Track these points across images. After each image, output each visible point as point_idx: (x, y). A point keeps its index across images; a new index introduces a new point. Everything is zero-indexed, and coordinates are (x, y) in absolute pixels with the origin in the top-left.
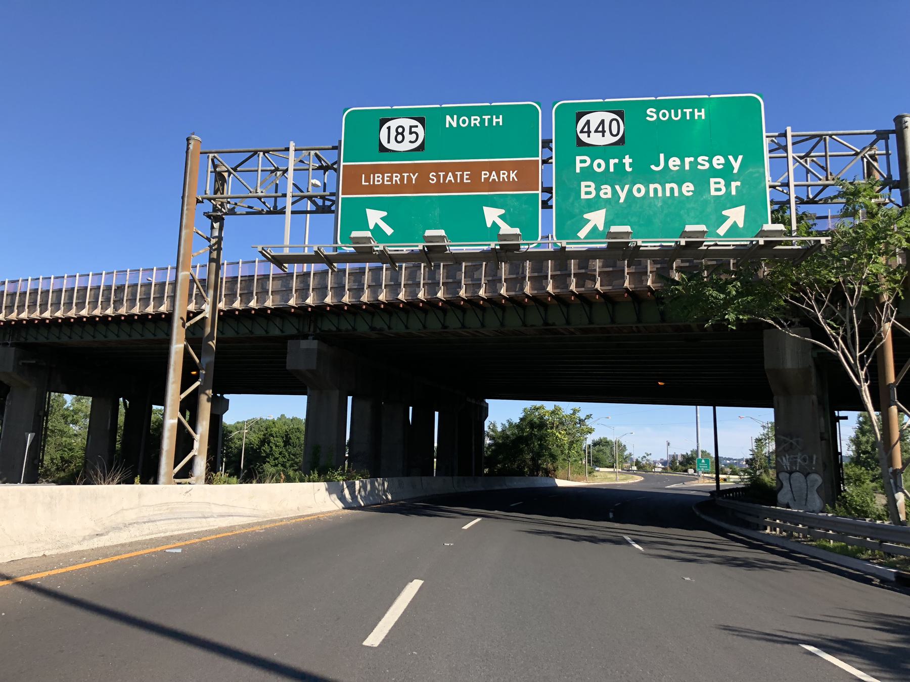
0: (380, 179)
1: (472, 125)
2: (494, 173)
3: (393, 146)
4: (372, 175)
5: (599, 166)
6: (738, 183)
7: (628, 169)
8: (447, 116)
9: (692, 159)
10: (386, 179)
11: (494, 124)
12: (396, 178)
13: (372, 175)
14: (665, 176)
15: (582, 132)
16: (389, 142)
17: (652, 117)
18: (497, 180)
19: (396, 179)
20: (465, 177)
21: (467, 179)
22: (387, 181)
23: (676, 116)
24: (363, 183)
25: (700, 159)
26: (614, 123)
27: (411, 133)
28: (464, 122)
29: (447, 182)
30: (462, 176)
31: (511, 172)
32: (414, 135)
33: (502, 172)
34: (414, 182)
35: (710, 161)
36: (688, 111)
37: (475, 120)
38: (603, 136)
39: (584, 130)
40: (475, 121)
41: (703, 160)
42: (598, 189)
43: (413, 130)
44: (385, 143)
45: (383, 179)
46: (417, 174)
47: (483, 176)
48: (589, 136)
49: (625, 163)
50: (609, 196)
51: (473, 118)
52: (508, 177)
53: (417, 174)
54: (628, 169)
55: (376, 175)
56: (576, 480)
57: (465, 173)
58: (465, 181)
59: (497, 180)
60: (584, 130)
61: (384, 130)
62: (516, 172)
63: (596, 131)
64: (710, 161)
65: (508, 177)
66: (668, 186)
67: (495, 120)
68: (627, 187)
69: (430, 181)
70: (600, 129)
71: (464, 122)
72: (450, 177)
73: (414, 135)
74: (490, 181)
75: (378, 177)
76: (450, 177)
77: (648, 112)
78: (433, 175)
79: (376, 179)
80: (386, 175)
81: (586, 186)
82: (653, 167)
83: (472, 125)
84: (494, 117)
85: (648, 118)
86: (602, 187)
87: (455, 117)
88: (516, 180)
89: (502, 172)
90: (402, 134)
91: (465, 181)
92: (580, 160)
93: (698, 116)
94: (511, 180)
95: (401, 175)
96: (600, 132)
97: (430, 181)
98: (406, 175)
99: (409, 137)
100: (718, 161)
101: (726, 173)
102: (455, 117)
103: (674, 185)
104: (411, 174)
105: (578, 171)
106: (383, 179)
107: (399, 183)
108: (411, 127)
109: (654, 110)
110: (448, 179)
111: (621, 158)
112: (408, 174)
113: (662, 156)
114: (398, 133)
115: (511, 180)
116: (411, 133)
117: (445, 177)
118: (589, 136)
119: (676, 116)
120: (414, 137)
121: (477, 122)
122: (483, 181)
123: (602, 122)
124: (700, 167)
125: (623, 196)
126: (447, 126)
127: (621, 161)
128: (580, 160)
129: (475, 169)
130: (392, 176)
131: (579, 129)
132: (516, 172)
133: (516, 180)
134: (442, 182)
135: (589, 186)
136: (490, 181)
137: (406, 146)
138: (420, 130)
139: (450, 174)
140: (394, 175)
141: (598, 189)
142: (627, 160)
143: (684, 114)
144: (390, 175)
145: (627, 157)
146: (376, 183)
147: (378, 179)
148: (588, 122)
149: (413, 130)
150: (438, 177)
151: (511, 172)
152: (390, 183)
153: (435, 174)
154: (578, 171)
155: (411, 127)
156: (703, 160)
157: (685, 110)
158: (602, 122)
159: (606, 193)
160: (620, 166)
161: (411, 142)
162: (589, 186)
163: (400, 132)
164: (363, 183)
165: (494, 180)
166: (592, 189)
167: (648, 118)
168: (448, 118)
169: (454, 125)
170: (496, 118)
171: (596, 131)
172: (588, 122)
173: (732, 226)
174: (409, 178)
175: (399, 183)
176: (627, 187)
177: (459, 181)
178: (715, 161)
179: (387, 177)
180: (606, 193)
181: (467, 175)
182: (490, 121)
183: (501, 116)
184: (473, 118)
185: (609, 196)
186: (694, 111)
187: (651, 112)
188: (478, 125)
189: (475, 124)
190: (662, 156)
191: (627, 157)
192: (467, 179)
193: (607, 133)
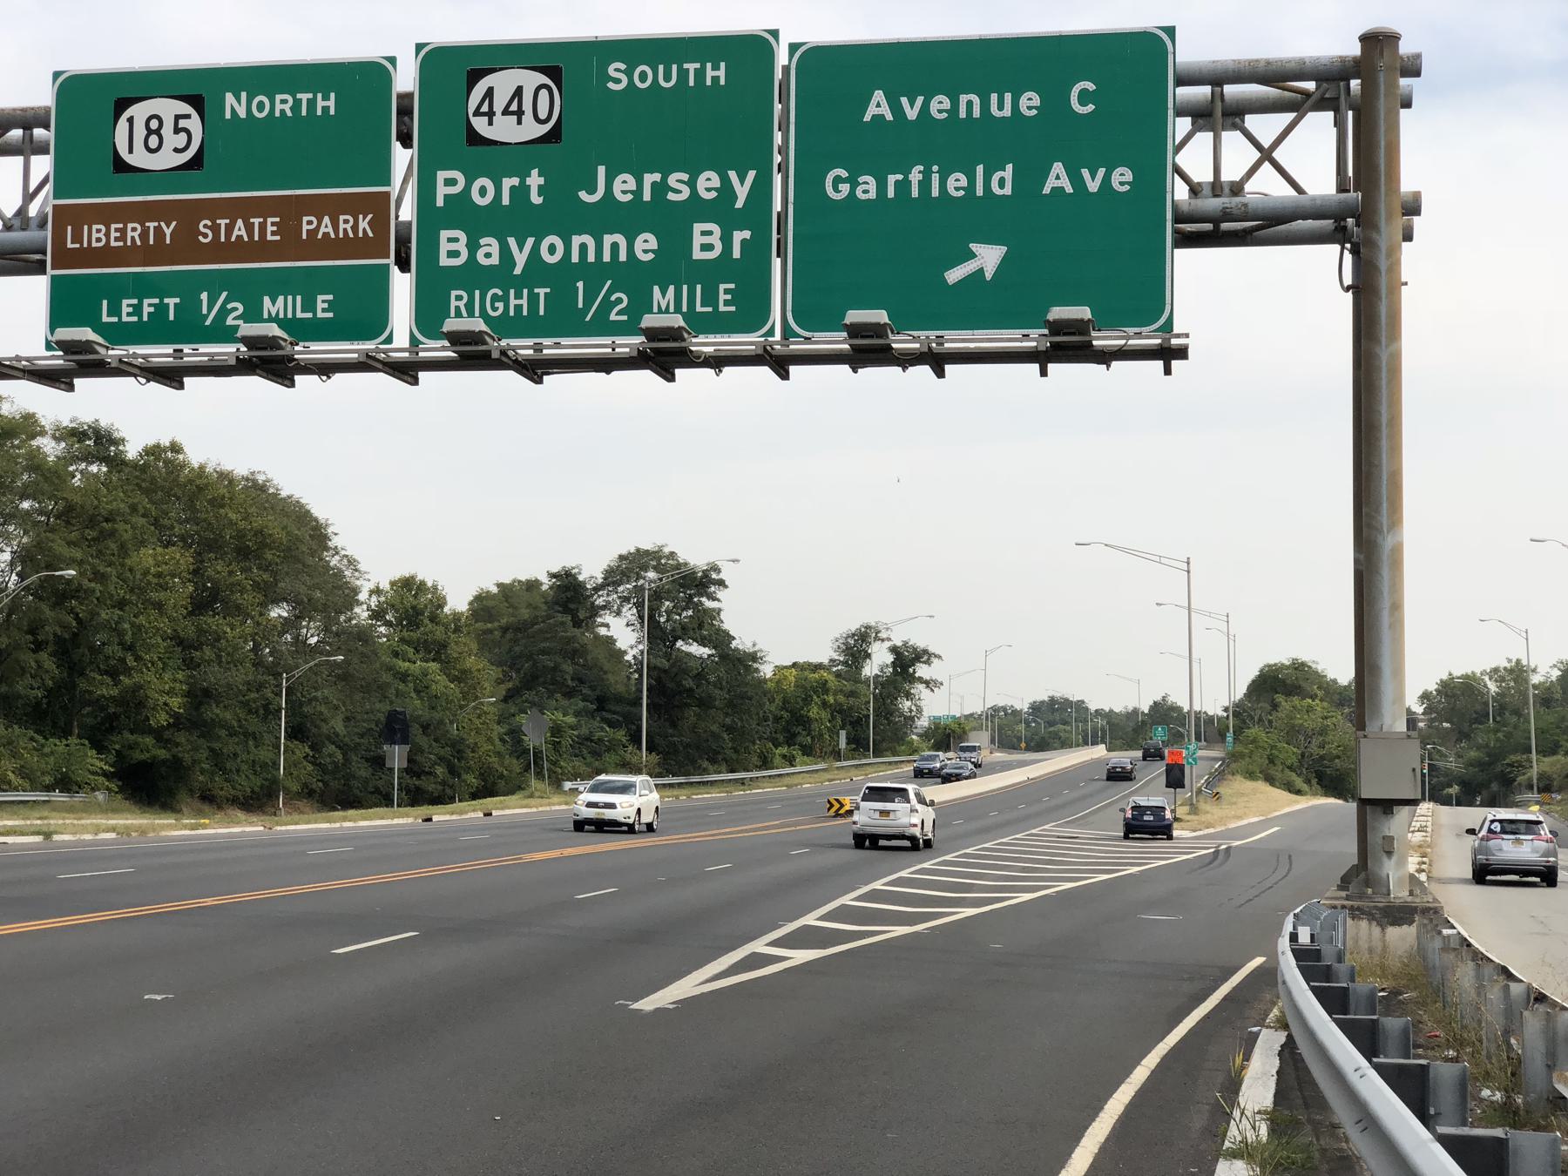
0: (101, 235)
1: (277, 114)
2: (326, 219)
3: (139, 158)
4: (86, 227)
5: (483, 192)
6: (747, 234)
7: (536, 199)
8: (227, 94)
9: (657, 177)
10: (114, 235)
11: (709, 82)
12: (134, 232)
13: (86, 227)
14: (609, 216)
15: (477, 113)
16: (131, 151)
17: (618, 81)
18: (333, 236)
19: (458, 303)
20: (270, 228)
21: (273, 233)
22: (116, 239)
23: (667, 78)
24: (70, 245)
25: (672, 180)
26: (544, 93)
27: (177, 130)
28: (261, 106)
29: (233, 239)
30: (263, 227)
31: (361, 217)
32: (183, 136)
33: (342, 218)
34: (168, 242)
35: (692, 184)
36: (692, 67)
37: (284, 102)
38: (519, 122)
39: (511, 109)
40: (283, 104)
41: (677, 181)
42: (473, 246)
43: (182, 123)
44: (123, 151)
45: (107, 235)
46: (174, 223)
47: (305, 227)
48: (490, 123)
49: (530, 186)
50: (495, 260)
51: (279, 97)
52: (355, 228)
53: (174, 223)
54: (536, 199)
55: (95, 227)
56: (222, 788)
57: (270, 220)
58: (270, 237)
59: (333, 236)
60: (511, 109)
61: (122, 124)
62: (370, 216)
63: (506, 112)
64: (692, 184)
65: (355, 228)
66: (608, 240)
67: (710, 73)
68: (530, 241)
69: (201, 238)
70: (514, 107)
71: (261, 106)
72: (240, 230)
73: (183, 136)
74: (320, 236)
75: (99, 231)
76: (240, 230)
77: (611, 71)
78: (205, 226)
79: (95, 235)
80: (113, 226)
81: (450, 240)
82: (583, 195)
83: (277, 114)
84: (709, 65)
85: (611, 85)
86: (483, 241)
87: (244, 95)
88: (371, 235)
89: (342, 218)
90: (158, 132)
91: (270, 237)
92: (445, 179)
93: (718, 69)
94: (361, 235)
95: (142, 225)
96: (513, 113)
97: (201, 238)
98: (152, 225)
99: (172, 140)
100: (708, 183)
101: (721, 210)
102: (244, 95)
103: (620, 239)
104: (163, 224)
106: (107, 235)
107: (139, 243)
108: (178, 118)
109: (623, 67)
110: (236, 233)
112: (156, 224)
113: (601, 170)
114: (150, 132)
115: (361, 235)
116: (177, 130)
117: (230, 228)
118: (490, 123)
119: (667, 78)
120: (181, 139)
121: (287, 107)
122: (304, 237)
123: (519, 92)
124: (671, 196)
125: (521, 259)
126: (228, 116)
127: (523, 182)
128: (445, 179)
129: (291, 211)
130: (125, 228)
131: (471, 112)
132: (370, 216)
133: (371, 235)
134: (223, 239)
135: (456, 240)
136: (320, 236)
137: (167, 159)
138: (194, 124)
139: (240, 223)
140: (130, 226)
141: (473, 246)
142: (535, 180)
143: (683, 74)
144: (121, 226)
145: (535, 172)
146: (94, 244)
147: (98, 235)
148: (490, 93)
149: (182, 123)
150: (215, 229)
151: (361, 217)
152: (121, 244)
153: (209, 223)
155: (178, 118)
156: (677, 181)
157: (686, 66)
158: (519, 92)
159: (488, 255)
160: (520, 192)
161: (176, 150)
162: (456, 240)
163: (154, 129)
164: (70, 245)
165: (326, 235)
166: (461, 247)
167: (611, 85)
169: (242, 113)
171: (506, 112)
172: (490, 93)
173: (386, 264)
174: (158, 230)
175: (139, 243)
176: (530, 241)
177: (256, 238)
178: (701, 184)
180: (488, 255)
181: (273, 224)
182: (700, 74)
183: (723, 65)
184: (279, 97)
185: (495, 260)
187: (617, 70)
188: (289, 114)
190: (601, 170)
191: (535, 172)
192: (273, 233)
193: (528, 116)
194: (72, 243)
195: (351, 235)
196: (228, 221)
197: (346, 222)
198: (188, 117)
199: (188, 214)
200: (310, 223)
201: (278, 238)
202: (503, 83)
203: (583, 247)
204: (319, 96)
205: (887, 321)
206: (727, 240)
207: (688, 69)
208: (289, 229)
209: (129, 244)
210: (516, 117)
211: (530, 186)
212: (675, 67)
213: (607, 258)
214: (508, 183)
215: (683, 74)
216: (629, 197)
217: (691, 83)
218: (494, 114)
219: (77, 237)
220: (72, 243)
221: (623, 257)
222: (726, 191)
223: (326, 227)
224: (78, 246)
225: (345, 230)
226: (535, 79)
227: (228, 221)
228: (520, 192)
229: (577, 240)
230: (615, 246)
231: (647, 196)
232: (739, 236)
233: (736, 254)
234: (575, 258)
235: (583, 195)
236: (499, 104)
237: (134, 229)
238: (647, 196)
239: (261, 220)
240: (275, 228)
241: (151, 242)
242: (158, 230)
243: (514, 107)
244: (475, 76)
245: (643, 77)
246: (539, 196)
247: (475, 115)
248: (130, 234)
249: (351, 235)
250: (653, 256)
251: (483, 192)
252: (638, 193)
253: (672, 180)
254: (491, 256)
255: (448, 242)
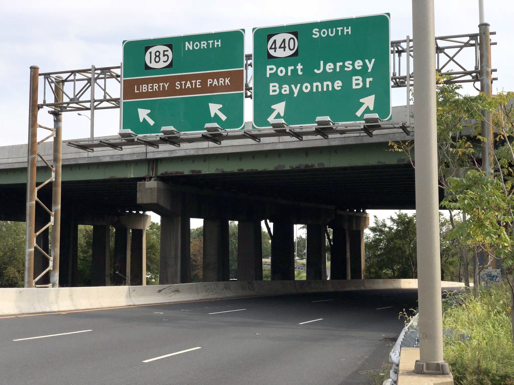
0: (146, 88)
1: (202, 48)
2: (215, 80)
3: (153, 65)
4: (141, 86)
5: (281, 72)
6: (371, 79)
7: (300, 73)
9: (341, 64)
10: (149, 88)
12: (156, 86)
13: (141, 86)
14: (325, 77)
15: (271, 48)
16: (151, 63)
17: (316, 35)
18: (217, 85)
20: (198, 84)
21: (199, 85)
22: (150, 89)
23: (332, 33)
24: (136, 92)
25: (346, 64)
26: (292, 41)
27: (164, 55)
28: (197, 46)
30: (196, 83)
31: (226, 79)
32: (166, 57)
33: (220, 79)
35: (353, 65)
36: (340, 29)
38: (284, 50)
42: (280, 88)
43: (166, 53)
45: (148, 88)
46: (168, 83)
47: (209, 83)
48: (275, 51)
49: (298, 69)
50: (288, 92)
51: (202, 43)
52: (224, 82)
53: (168, 83)
54: (300, 73)
55: (144, 86)
57: (198, 81)
58: (198, 87)
59: (217, 85)
61: (148, 55)
63: (280, 47)
64: (353, 65)
65: (224, 82)
66: (325, 84)
67: (346, 30)
68: (299, 85)
69: (176, 88)
70: (283, 46)
72: (188, 84)
73: (166, 57)
74: (213, 85)
75: (145, 87)
76: (188, 84)
77: (314, 32)
78: (178, 84)
79: (144, 88)
80: (149, 85)
82: (316, 71)
83: (202, 48)
85: (314, 36)
86: (283, 86)
88: (229, 84)
89: (220, 79)
90: (159, 56)
91: (198, 87)
94: (226, 84)
95: (158, 84)
96: (282, 48)
97: (176, 88)
98: (161, 84)
100: (358, 64)
101: (363, 72)
103: (329, 83)
104: (165, 84)
105: (268, 76)
106: (148, 88)
107: (157, 90)
108: (164, 51)
109: (318, 30)
110: (187, 85)
111: (295, 65)
112: (163, 84)
113: (322, 62)
114: (156, 56)
115: (226, 84)
116: (164, 55)
117: (185, 84)
118: (275, 51)
119: (332, 33)
121: (205, 45)
122: (209, 86)
124: (346, 69)
125: (296, 91)
129: (204, 78)
130: (153, 85)
131: (269, 47)
132: (229, 78)
133: (229, 84)
134: (183, 88)
135: (275, 86)
136: (213, 85)
137: (161, 65)
138: (170, 53)
139: (189, 82)
140: (155, 85)
141: (280, 88)
142: (299, 67)
143: (337, 31)
144: (152, 85)
145: (299, 64)
146: (144, 91)
148: (275, 42)
149: (166, 53)
150: (181, 85)
151: (226, 79)
152: (152, 90)
153: (179, 83)
154: (268, 76)
155: (164, 51)
157: (338, 29)
158: (284, 41)
159: (285, 91)
160: (294, 71)
161: (164, 62)
164: (136, 92)
166: (277, 88)
167: (314, 36)
168: (187, 43)
170: (219, 44)
171: (280, 47)
172: (275, 42)
174: (163, 86)
175: (157, 90)
176: (299, 85)
177: (194, 87)
179: (150, 86)
180: (285, 91)
181: (199, 82)
184: (202, 43)
185: (288, 92)
186: (344, 28)
188: (206, 47)
189: (204, 47)
190: (322, 62)
191: (299, 64)
192: (199, 85)
194: (137, 91)
195: (223, 85)
196: (185, 82)
197: (222, 80)
198: (167, 51)
199: (172, 80)
200: (210, 81)
201: (200, 86)
202: (279, 38)
203: (317, 86)
204: (216, 41)
205: (378, 117)
206: (364, 82)
207: (210, 43)
208: (204, 83)
209: (154, 90)
210: (274, 50)
211: (298, 69)
212: (334, 29)
213: (325, 89)
214: (290, 68)
215: (337, 31)
216: (331, 71)
217: (340, 34)
218: (276, 48)
219: (138, 89)
220: (137, 91)
221: (330, 89)
222: (365, 66)
223: (215, 82)
224: (138, 92)
225: (221, 83)
226: (289, 36)
227: (185, 82)
228: (294, 71)
229: (315, 84)
230: (328, 86)
231: (338, 70)
232: (368, 80)
233: (368, 86)
234: (314, 90)
235: (316, 71)
236: (278, 45)
237: (156, 86)
238: (338, 70)
239: (195, 81)
240: (199, 84)
241: (161, 90)
242: (163, 86)
243: (283, 46)
244: (270, 37)
245: (324, 33)
246: (301, 72)
247: (279, 48)
248: (154, 87)
249: (223, 85)
250: (341, 88)
251: (281, 72)
252: (335, 68)
253: (346, 64)
254: (284, 91)
255: (272, 87)
